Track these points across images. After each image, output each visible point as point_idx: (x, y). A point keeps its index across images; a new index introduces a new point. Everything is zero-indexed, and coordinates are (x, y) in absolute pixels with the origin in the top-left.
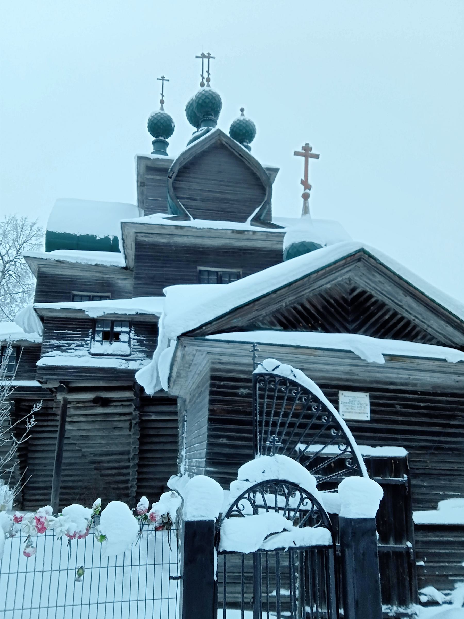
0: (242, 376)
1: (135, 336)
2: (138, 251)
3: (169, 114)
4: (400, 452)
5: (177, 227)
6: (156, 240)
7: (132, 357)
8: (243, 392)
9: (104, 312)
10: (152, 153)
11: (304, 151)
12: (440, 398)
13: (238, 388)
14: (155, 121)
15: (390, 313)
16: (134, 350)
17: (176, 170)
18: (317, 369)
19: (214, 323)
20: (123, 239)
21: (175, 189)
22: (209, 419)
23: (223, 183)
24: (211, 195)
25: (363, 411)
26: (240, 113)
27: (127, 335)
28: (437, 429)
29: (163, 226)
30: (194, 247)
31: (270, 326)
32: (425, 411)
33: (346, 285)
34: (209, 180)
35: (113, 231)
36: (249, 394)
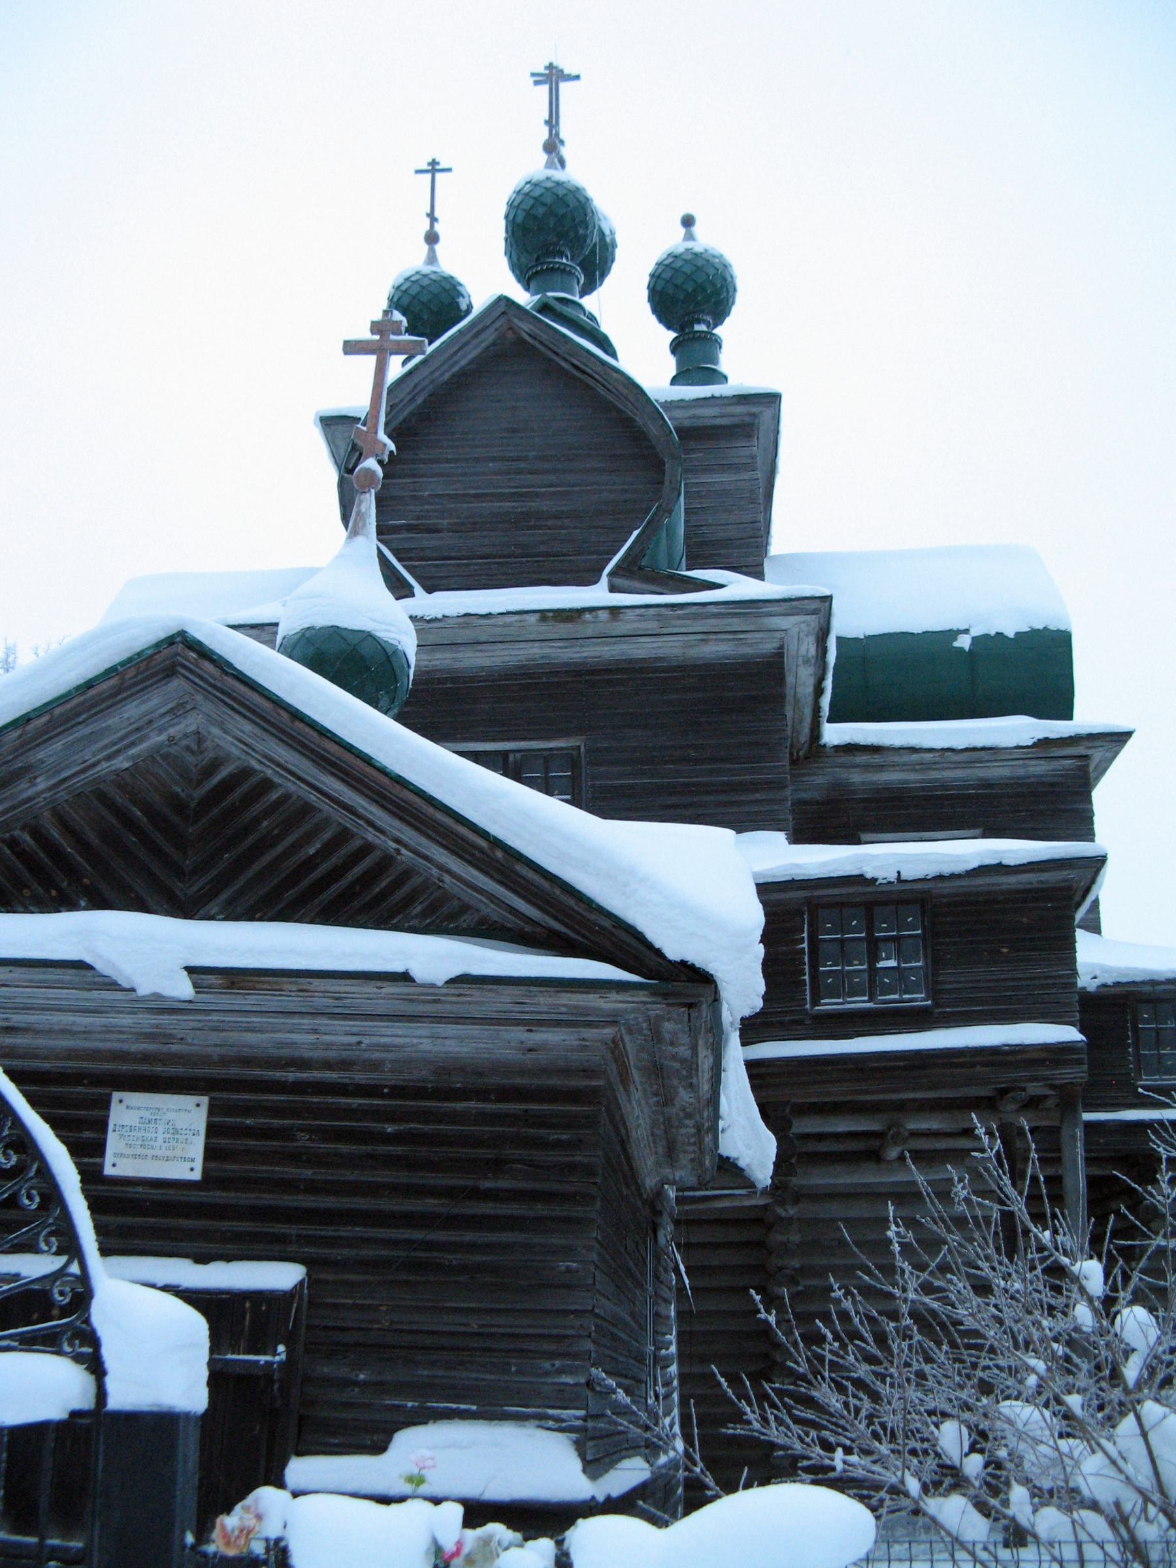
4: (281, 1276)
11: (377, 337)
12: (460, 1106)
15: (327, 835)
18: (56, 1027)
23: (522, 465)
24: (485, 506)
25: (178, 1153)
26: (683, 231)
28: (431, 1204)
32: (398, 1150)
33: (190, 759)
34: (477, 460)
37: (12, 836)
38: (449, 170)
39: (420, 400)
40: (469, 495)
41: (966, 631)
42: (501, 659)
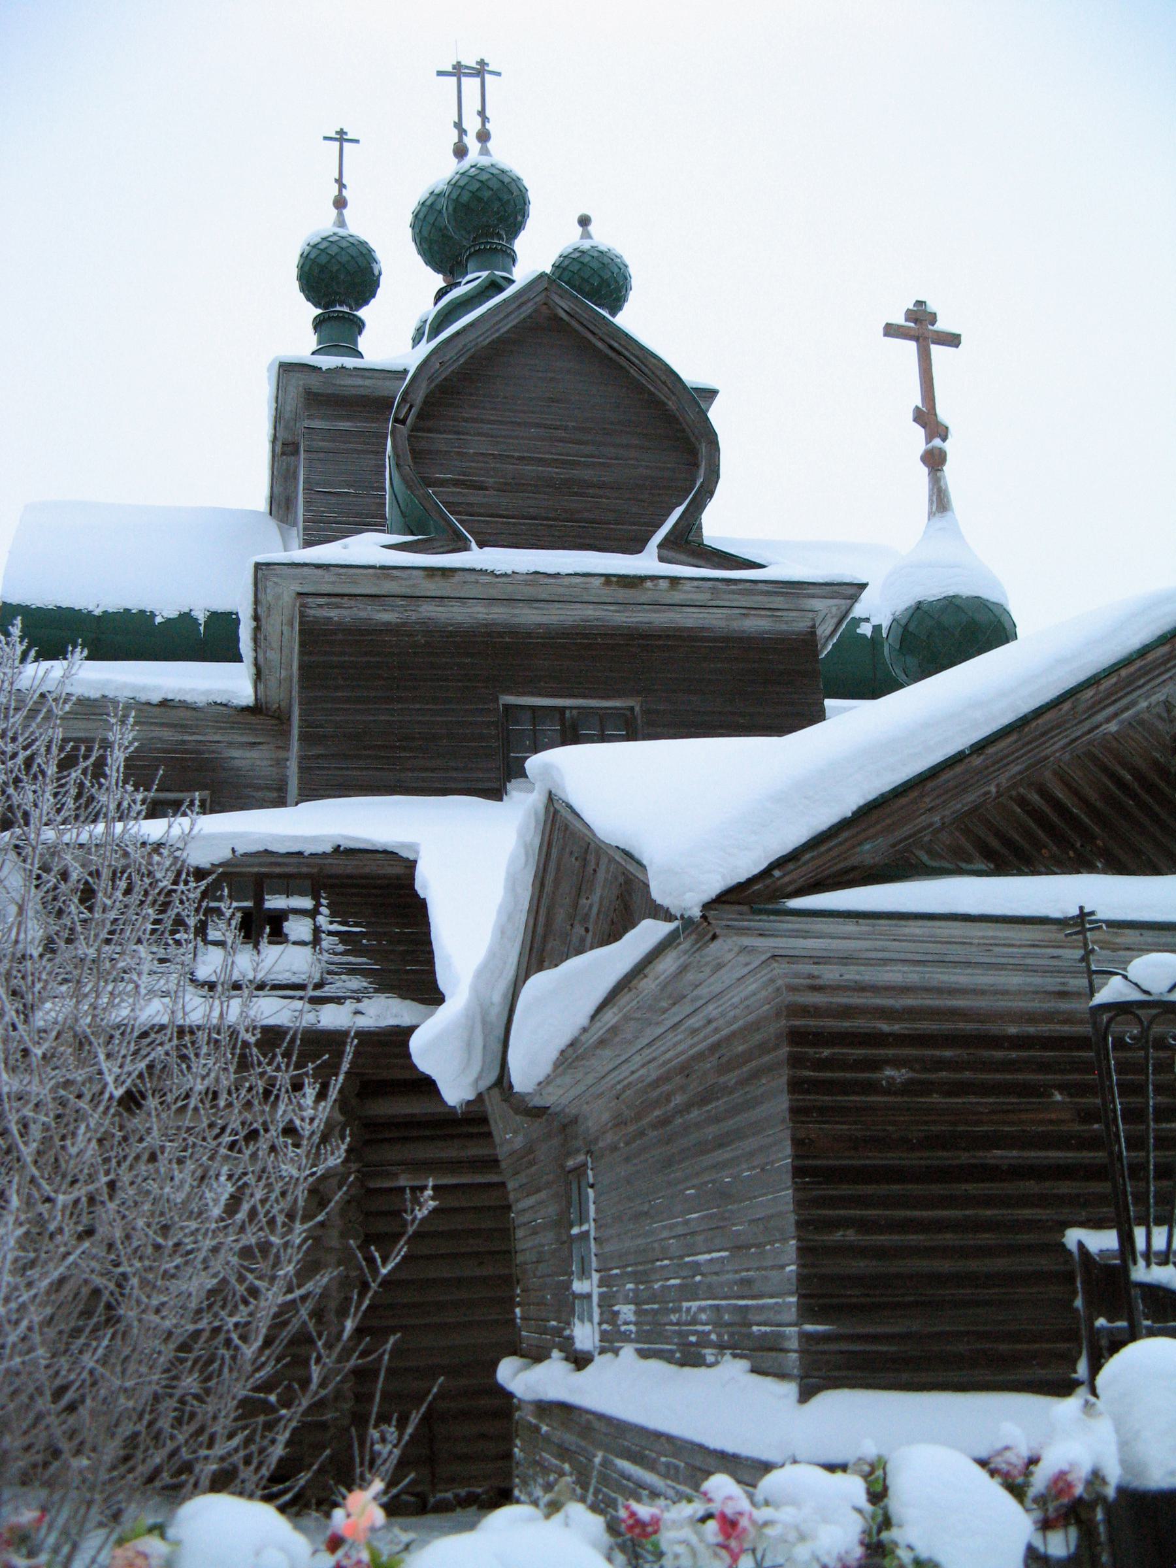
0: (885, 1027)
1: (331, 923)
2: (310, 653)
3: (364, 237)
5: (432, 572)
6: (363, 614)
7: (327, 991)
8: (893, 1078)
9: (233, 851)
10: (313, 353)
13: (876, 1065)
14: (323, 259)
16: (332, 967)
17: (419, 398)
19: (807, 856)
20: (256, 618)
21: (417, 455)
22: (798, 1172)
24: (529, 469)
27: (308, 922)
29: (386, 570)
30: (489, 635)
31: (955, 862)
33: (1160, 726)
35: (235, 596)
36: (911, 1082)
37: (1019, 794)
38: (357, 141)
39: (462, 361)
40: (513, 457)
41: (867, 620)
42: (557, 618)
